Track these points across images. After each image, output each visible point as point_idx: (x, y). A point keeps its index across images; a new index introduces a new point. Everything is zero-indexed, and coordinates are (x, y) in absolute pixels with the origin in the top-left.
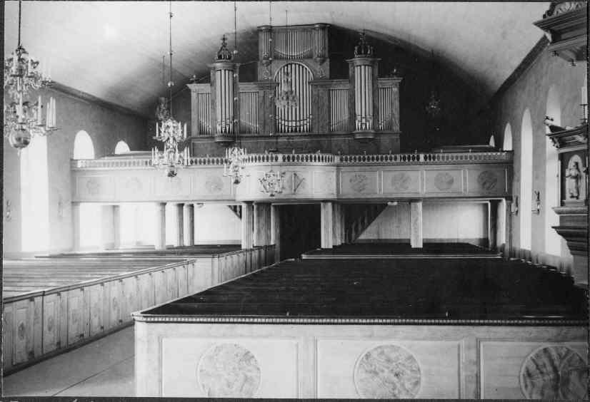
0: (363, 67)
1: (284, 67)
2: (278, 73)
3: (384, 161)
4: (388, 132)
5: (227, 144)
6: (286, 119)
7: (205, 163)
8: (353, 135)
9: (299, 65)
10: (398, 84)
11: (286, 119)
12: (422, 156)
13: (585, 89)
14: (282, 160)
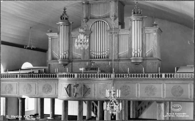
0: (136, 21)
1: (95, 23)
2: (92, 26)
3: (143, 77)
4: (150, 58)
5: (65, 65)
6: (95, 51)
7: (36, 77)
8: (130, 60)
9: (103, 21)
10: (157, 31)
11: (95, 51)
12: (163, 75)
13: (148, 1)
14: (77, 77)
